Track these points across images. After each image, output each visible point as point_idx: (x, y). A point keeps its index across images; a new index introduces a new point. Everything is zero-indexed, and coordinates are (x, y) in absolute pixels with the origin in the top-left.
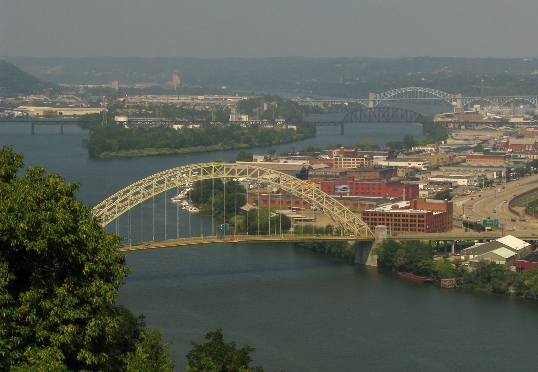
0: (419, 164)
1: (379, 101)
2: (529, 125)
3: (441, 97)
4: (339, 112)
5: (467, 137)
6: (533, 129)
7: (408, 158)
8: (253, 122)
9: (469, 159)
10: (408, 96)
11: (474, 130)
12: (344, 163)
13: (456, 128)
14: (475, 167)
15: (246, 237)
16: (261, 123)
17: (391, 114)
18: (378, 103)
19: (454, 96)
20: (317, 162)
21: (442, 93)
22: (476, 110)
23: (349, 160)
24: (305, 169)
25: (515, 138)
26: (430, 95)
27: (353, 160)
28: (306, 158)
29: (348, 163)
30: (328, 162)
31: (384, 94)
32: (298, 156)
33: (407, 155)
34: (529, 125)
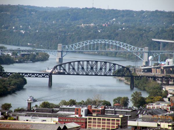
0: (169, 126)
10: (92, 49)
12: (113, 124)
13: (164, 84)
17: (99, 67)
19: (142, 50)
21: (130, 46)
22: (168, 65)
23: (104, 120)
27: (113, 120)
29: (102, 123)
30: (79, 121)
32: (35, 112)
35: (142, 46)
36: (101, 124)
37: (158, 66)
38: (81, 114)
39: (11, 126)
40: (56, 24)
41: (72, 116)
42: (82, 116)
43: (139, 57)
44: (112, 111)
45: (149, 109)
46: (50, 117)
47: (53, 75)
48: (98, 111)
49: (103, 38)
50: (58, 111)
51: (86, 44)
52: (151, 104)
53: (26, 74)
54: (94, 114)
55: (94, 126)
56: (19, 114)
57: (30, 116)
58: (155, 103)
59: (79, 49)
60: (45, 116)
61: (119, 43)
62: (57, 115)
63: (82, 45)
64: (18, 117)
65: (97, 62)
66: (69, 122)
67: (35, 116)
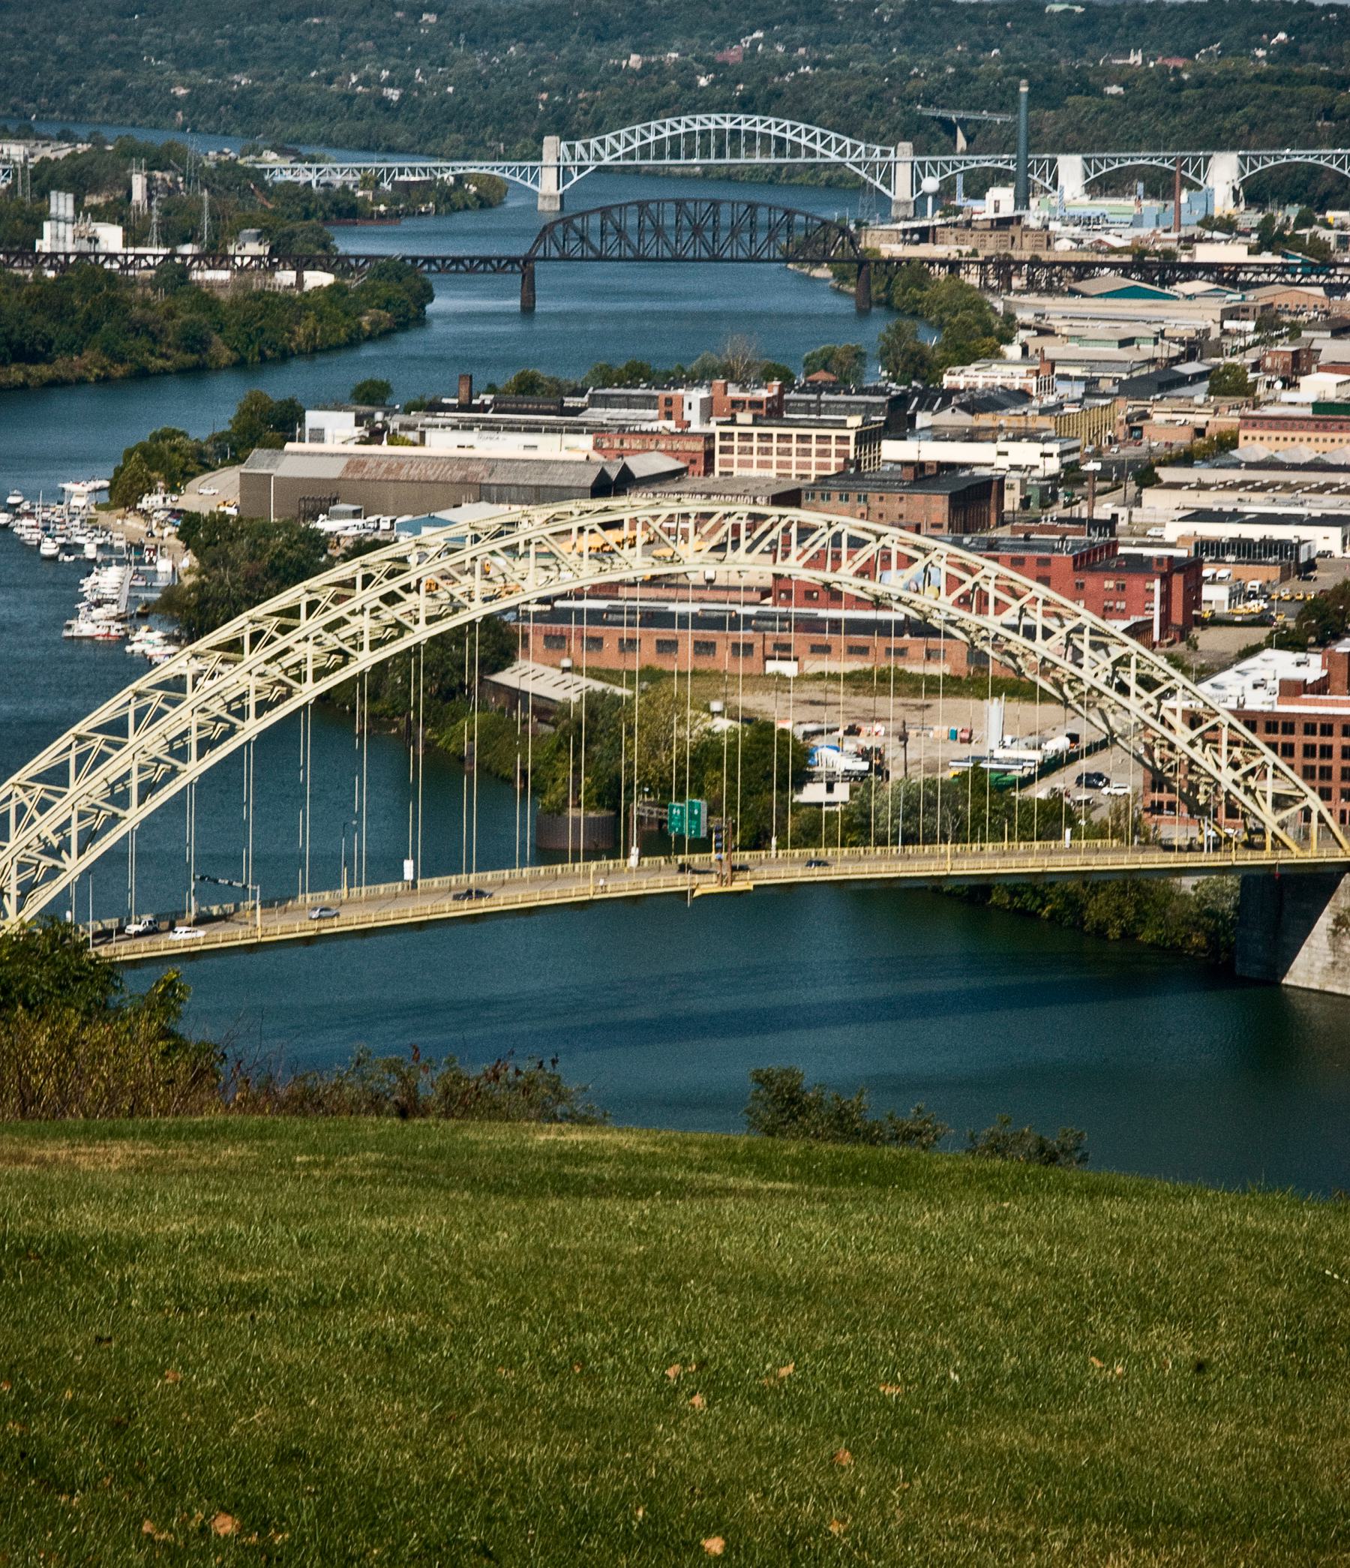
1: (581, 169)
2: (1294, 275)
3: (833, 157)
4: (427, 213)
5: (1127, 330)
6: (1320, 291)
7: (976, 424)
8: (155, 256)
9: (1250, 433)
11: (1073, 293)
14: (1295, 467)
15: (770, 863)
16: (72, 259)
18: (576, 178)
20: (626, 445)
22: (997, 210)
23: (787, 438)
24: (608, 477)
25: (1328, 334)
26: (788, 147)
28: (536, 423)
31: (602, 143)
33: (972, 413)
34: (1294, 275)
35: (888, 139)
36: (774, 458)
37: (960, 217)
38: (686, 418)
39: (404, 471)
40: (524, 60)
41: (646, 427)
42: (689, 424)
43: (877, 184)
44: (809, 402)
45: (955, 391)
46: (554, 431)
47: (538, 266)
48: (756, 404)
49: (722, 107)
50: (582, 409)
51: (643, 138)
52: (958, 369)
53: (430, 260)
54: (745, 417)
55: (742, 464)
56: (428, 420)
57: (471, 428)
58: (974, 366)
59: (630, 155)
60: (533, 429)
61: (793, 128)
62: (584, 424)
63: (628, 143)
64: (423, 434)
65: (715, 203)
66: (639, 451)
67: (492, 429)
